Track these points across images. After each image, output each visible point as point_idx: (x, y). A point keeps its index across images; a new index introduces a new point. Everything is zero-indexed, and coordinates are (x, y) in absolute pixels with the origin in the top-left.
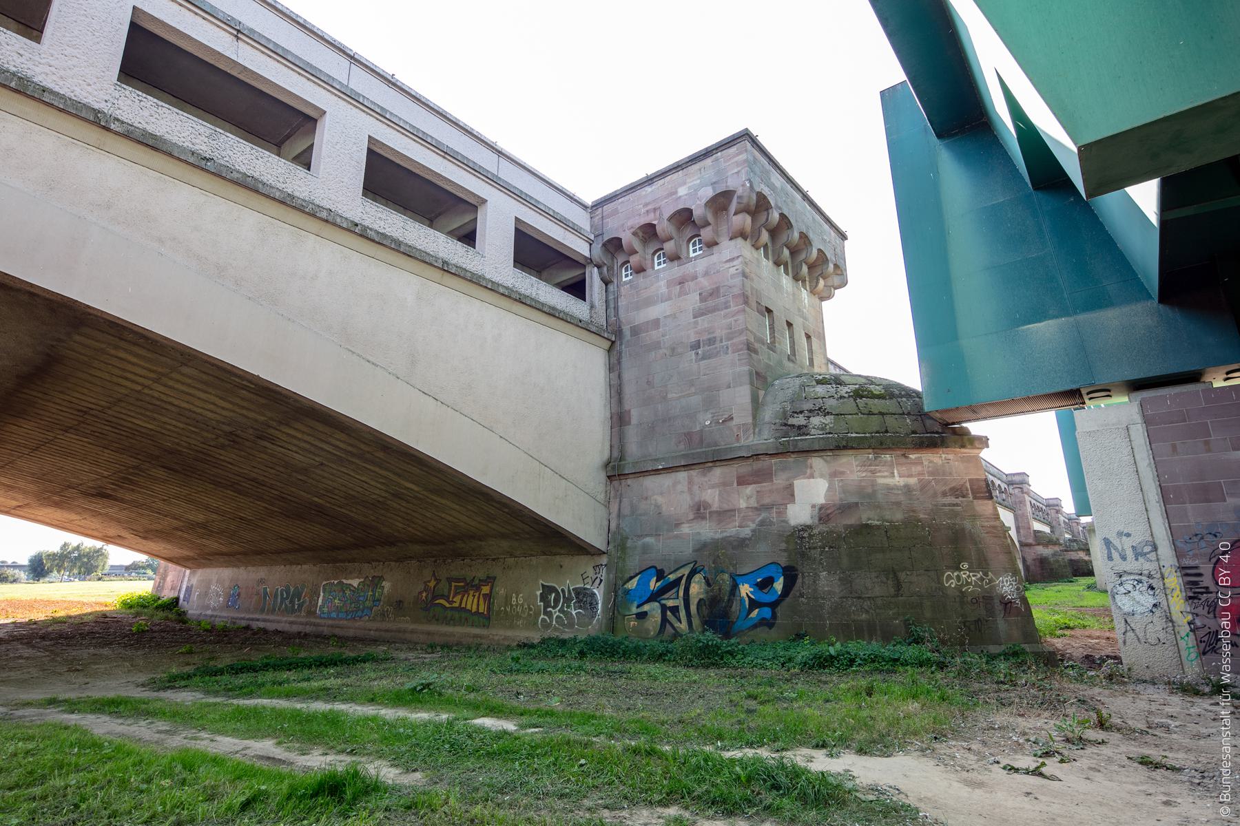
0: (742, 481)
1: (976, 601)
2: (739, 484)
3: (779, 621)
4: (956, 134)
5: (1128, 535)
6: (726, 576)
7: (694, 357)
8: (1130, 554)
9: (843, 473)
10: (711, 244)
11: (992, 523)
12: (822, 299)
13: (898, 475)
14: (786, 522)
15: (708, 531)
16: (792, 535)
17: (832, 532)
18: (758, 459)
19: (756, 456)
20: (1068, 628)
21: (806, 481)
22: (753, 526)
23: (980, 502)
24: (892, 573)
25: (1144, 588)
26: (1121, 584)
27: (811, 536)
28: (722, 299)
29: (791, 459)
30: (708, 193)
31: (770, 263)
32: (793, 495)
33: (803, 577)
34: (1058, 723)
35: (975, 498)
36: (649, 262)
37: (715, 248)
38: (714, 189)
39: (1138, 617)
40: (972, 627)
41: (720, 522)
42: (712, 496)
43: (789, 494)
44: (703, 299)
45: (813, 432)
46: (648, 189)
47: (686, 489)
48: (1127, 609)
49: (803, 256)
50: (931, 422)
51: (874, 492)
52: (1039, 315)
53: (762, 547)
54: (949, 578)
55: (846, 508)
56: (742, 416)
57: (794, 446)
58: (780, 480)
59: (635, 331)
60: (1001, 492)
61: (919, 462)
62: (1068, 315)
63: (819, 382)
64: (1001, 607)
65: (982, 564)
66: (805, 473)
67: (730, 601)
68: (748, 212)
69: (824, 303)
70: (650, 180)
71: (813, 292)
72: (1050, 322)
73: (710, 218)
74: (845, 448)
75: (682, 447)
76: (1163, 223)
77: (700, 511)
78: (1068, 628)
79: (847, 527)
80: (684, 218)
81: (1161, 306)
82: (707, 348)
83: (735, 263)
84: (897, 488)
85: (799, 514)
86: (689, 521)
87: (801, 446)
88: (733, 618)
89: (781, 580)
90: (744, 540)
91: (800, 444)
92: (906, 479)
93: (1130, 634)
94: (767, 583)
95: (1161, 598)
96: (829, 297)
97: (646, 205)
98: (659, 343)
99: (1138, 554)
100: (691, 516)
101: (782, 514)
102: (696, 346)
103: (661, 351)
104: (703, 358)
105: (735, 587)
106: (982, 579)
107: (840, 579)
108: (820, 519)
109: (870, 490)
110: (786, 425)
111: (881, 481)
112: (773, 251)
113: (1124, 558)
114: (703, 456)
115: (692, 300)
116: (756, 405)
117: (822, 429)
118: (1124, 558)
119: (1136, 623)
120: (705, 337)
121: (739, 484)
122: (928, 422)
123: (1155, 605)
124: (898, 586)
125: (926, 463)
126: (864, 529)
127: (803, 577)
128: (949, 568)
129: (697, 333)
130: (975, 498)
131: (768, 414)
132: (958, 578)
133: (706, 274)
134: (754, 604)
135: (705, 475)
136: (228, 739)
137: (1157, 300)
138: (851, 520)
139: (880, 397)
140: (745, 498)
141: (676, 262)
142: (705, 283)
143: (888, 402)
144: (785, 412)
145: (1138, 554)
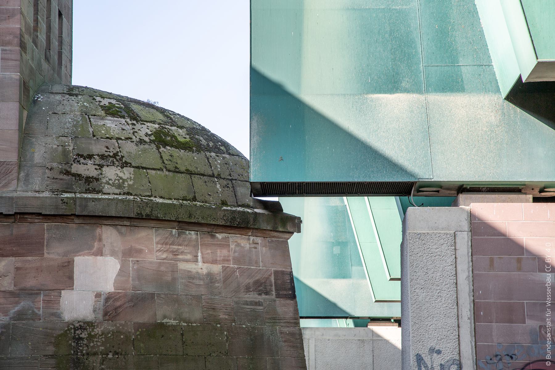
9: (140, 251)
11: (292, 329)
13: (202, 261)
14: (58, 316)
16: (65, 334)
17: (119, 332)
21: (91, 258)
29: (73, 226)
32: (71, 278)
35: (278, 296)
43: (66, 275)
45: (106, 188)
51: (174, 280)
55: (139, 301)
58: (54, 254)
62: (419, 91)
63: (110, 111)
66: (91, 247)
79: (138, 326)
84: (198, 276)
87: (94, 209)
91: (91, 204)
101: (53, 302)
108: (106, 314)
109: (169, 278)
110: (68, 173)
111: (182, 266)
117: (119, 186)
125: (232, 246)
130: (278, 296)
131: (40, 152)
138: (144, 318)
143: (196, 156)
144: (65, 153)
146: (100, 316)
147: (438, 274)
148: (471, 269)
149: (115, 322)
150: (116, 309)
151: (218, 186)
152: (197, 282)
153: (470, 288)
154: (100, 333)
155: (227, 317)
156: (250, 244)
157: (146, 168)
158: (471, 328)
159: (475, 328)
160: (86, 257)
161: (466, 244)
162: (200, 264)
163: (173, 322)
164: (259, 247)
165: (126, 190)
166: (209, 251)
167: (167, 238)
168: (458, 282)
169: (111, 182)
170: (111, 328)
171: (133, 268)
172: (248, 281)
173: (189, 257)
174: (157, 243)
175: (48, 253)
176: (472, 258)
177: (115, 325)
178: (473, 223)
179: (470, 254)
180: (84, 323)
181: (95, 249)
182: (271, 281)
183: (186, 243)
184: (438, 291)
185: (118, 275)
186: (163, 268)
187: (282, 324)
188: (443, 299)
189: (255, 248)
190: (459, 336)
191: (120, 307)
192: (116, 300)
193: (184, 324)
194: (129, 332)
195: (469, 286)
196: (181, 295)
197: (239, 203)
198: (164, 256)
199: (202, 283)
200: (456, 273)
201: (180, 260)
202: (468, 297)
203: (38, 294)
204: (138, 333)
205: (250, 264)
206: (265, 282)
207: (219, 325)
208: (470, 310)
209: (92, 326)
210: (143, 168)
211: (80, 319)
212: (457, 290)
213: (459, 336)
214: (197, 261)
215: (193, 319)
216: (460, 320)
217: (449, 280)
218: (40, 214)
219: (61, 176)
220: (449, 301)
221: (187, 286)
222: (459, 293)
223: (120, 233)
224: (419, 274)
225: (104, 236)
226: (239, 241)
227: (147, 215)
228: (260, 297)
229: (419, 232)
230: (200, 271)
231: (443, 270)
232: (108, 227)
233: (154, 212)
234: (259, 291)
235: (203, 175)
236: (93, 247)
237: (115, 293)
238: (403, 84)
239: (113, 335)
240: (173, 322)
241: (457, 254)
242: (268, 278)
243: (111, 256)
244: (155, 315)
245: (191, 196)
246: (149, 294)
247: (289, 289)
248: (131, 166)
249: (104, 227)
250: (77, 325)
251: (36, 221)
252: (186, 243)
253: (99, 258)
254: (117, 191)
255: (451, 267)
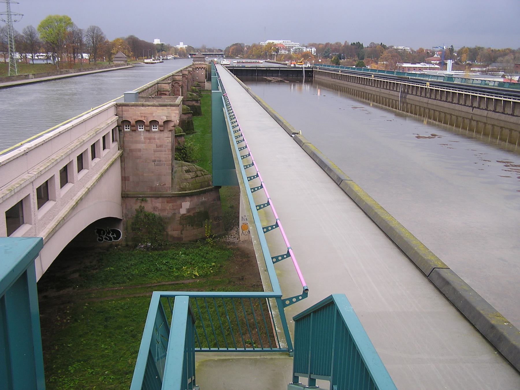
30: (165, 119)
34: (172, 124)
44: (157, 147)
85: (183, 211)
104: (157, 165)
115: (153, 146)
133: (159, 139)
136: (467, 281)
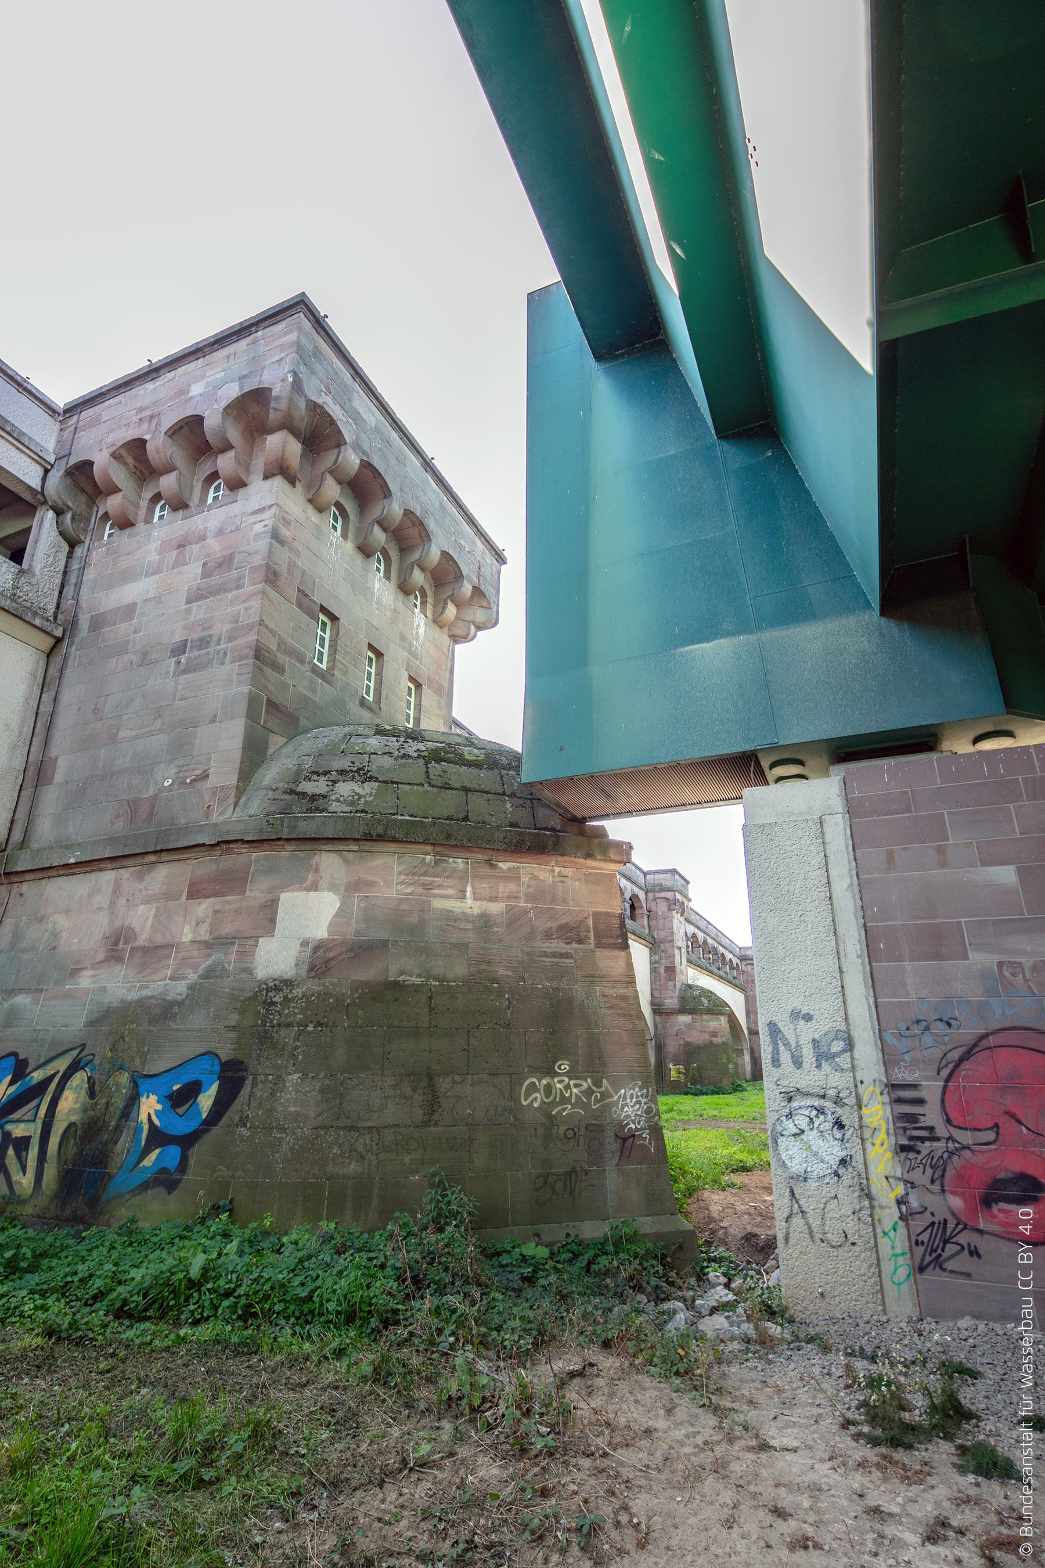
0: (196, 892)
1: (572, 1135)
2: (191, 896)
3: (189, 1177)
4: (622, 355)
5: (808, 1018)
6: (124, 1078)
7: (172, 668)
8: (808, 1054)
9: (372, 884)
10: (236, 485)
11: (622, 991)
12: (456, 639)
13: (469, 896)
14: (249, 971)
15: (119, 985)
16: (254, 998)
17: (328, 994)
18: (230, 851)
19: (223, 844)
20: (745, 1169)
21: (301, 894)
22: (193, 977)
23: (607, 952)
24: (426, 1081)
25: (827, 1126)
26: (790, 1115)
27: (287, 1001)
28: (234, 574)
29: (285, 853)
30: (233, 391)
31: (349, 546)
32: (273, 921)
33: (254, 1085)
35: (599, 945)
36: (142, 513)
37: (242, 492)
38: (241, 387)
39: (812, 1184)
40: (559, 1186)
41: (143, 967)
42: (142, 919)
44: (206, 574)
45: (334, 807)
46: (150, 386)
47: (106, 904)
48: (796, 1166)
49: (416, 556)
50: (547, 811)
51: (423, 922)
52: (709, 631)
53: (198, 1020)
54: (533, 1088)
55: (362, 950)
56: (224, 773)
57: (297, 832)
58: (256, 893)
59: (98, 623)
60: (732, 968)
61: (513, 876)
62: (748, 631)
64: (615, 1146)
65: (593, 1065)
67: (118, 1130)
68: (295, 432)
69: (457, 647)
70: (153, 372)
71: (437, 621)
72: (723, 642)
73: (234, 435)
74: (381, 838)
75: (119, 825)
76: (888, 353)
77: (118, 946)
78: (745, 1169)
79: (357, 986)
80: (191, 431)
81: (884, 620)
82: (196, 653)
83: (266, 515)
84: (465, 917)
85: (276, 957)
86: (96, 965)
88: (112, 1169)
89: (214, 1089)
90: (173, 1004)
92: (485, 904)
93: (797, 1221)
94: (182, 1098)
95: (854, 1148)
96: (465, 638)
97: (142, 409)
98: (127, 643)
99: (823, 1056)
100: (101, 956)
102: (180, 649)
103: (126, 658)
105: (133, 1100)
106: (589, 1092)
107: (322, 1091)
108: (311, 969)
109: (414, 919)
110: (292, 792)
111: (438, 904)
112: (400, 572)
113: (798, 1063)
114: (145, 846)
116: (254, 754)
118: (798, 1063)
119: (811, 1196)
120: (197, 634)
121: (191, 896)
122: (542, 812)
123: (843, 1162)
124: (433, 1104)
125: (525, 879)
126: (390, 991)
127: (254, 1085)
128: (534, 1070)
129: (185, 628)
130: (599, 945)
131: (271, 774)
132: (548, 1089)
133: (220, 532)
134: (157, 1137)
135: (140, 877)
137: (878, 612)
138: (368, 974)
139: (476, 765)
140: (193, 922)
141: (180, 513)
142: (215, 546)
143: (482, 774)
145: (823, 1056)
146: (304, 972)
147: (798, 886)
148: (854, 872)
149: (323, 981)
150: (327, 962)
151: (508, 805)
152: (463, 925)
153: (855, 905)
154: (300, 996)
155: (510, 973)
156: (553, 877)
157: (397, 783)
158: (864, 973)
159: (871, 973)
160: (296, 893)
161: (842, 833)
162: (469, 902)
163: (414, 979)
164: (569, 881)
165: (359, 808)
166: (486, 885)
167: (415, 867)
168: (834, 896)
169: (342, 799)
170: (316, 989)
171: (358, 905)
172: (549, 925)
173: (450, 892)
174: (400, 873)
175: (251, 890)
176: (854, 855)
177: (323, 984)
178: (852, 798)
179: (851, 848)
180: (281, 981)
181: (308, 882)
182: (588, 927)
183: (446, 874)
184: (800, 913)
185: (337, 915)
186: (405, 907)
187: (606, 984)
188: (810, 926)
189: (563, 882)
190: (843, 987)
191: (333, 959)
192: (330, 949)
193: (434, 983)
194: (343, 994)
195: (855, 901)
196: (432, 943)
197: (538, 826)
198: (409, 890)
199: (470, 926)
200: (829, 882)
201: (435, 896)
202: (853, 919)
203: (233, 943)
204: (356, 995)
205: (553, 900)
206: (577, 927)
207: (495, 985)
208: (859, 942)
209: (291, 985)
210: (393, 782)
211: (276, 976)
212: (832, 909)
213: (843, 987)
214: (464, 897)
215: (450, 976)
216: (843, 960)
217: (816, 893)
218: (243, 841)
219: (284, 797)
220: (821, 929)
221: (444, 930)
222: (837, 912)
223: (346, 861)
224: (766, 887)
225: (322, 866)
226: (536, 873)
227: (378, 835)
228: (568, 946)
229: (761, 823)
230: (468, 911)
231: (806, 878)
232: (330, 853)
233: (389, 831)
234: (567, 938)
235: (487, 793)
236: (307, 879)
237: (328, 940)
238: (724, 627)
239: (318, 998)
240: (414, 979)
241: (828, 851)
242: (581, 922)
243: (330, 891)
244: (387, 970)
245: (461, 815)
246: (380, 941)
247: (618, 937)
248: (377, 780)
249: (324, 855)
250: (271, 984)
251: (244, 851)
252: (446, 874)
253: (312, 893)
254: (348, 809)
255: (819, 871)
